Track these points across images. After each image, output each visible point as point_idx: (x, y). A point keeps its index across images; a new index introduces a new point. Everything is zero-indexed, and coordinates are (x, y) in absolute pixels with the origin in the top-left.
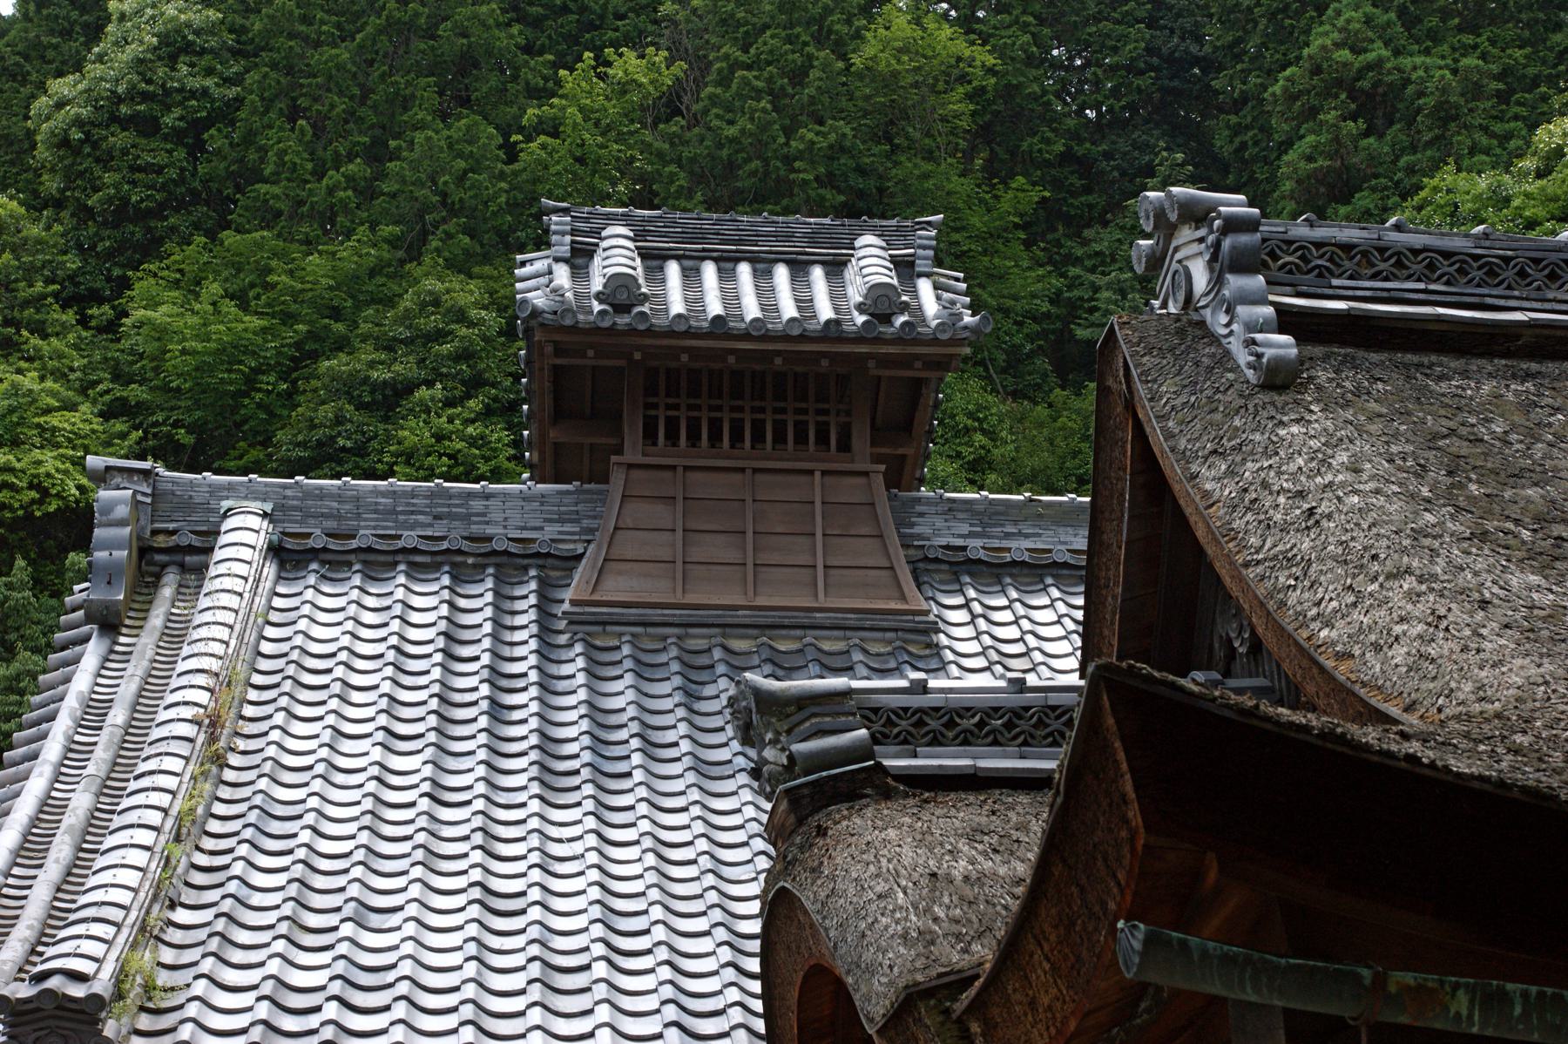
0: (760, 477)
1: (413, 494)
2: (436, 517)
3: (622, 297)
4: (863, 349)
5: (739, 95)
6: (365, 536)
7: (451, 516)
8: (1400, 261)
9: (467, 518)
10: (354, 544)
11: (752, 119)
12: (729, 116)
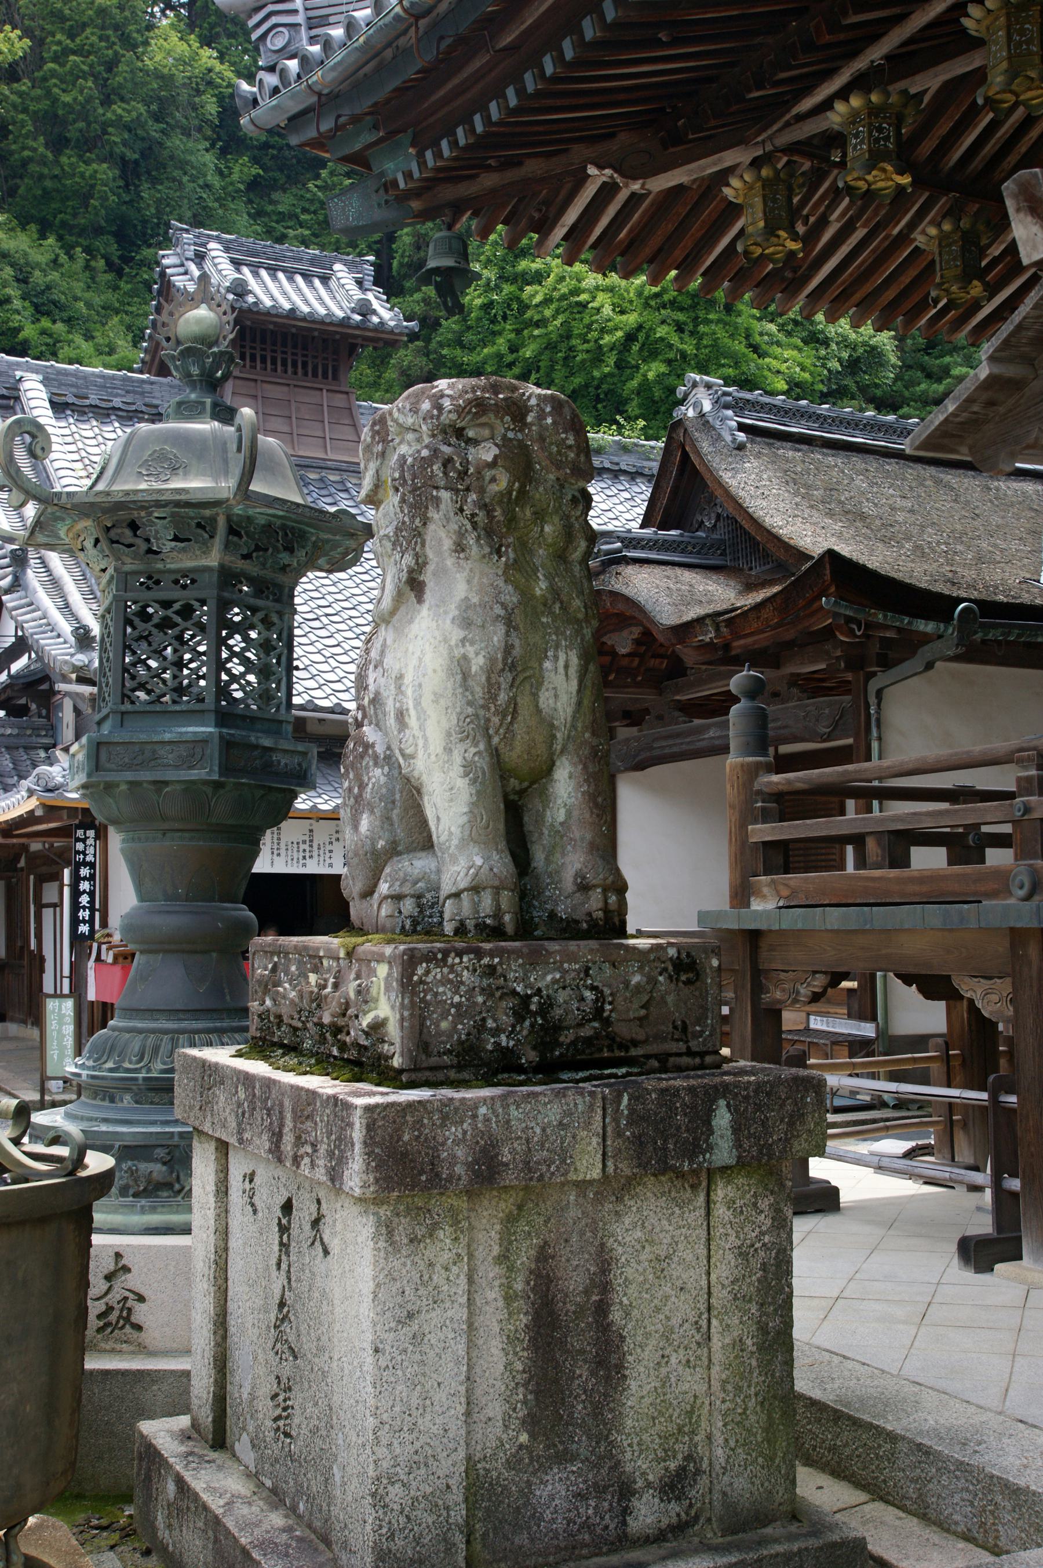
0: (265, 385)
1: (113, 378)
2: (128, 392)
3: (239, 290)
4: (357, 332)
5: (71, 73)
6: (93, 399)
7: (135, 392)
8: (762, 407)
9: (142, 393)
10: (87, 402)
11: (81, 92)
12: (64, 86)
